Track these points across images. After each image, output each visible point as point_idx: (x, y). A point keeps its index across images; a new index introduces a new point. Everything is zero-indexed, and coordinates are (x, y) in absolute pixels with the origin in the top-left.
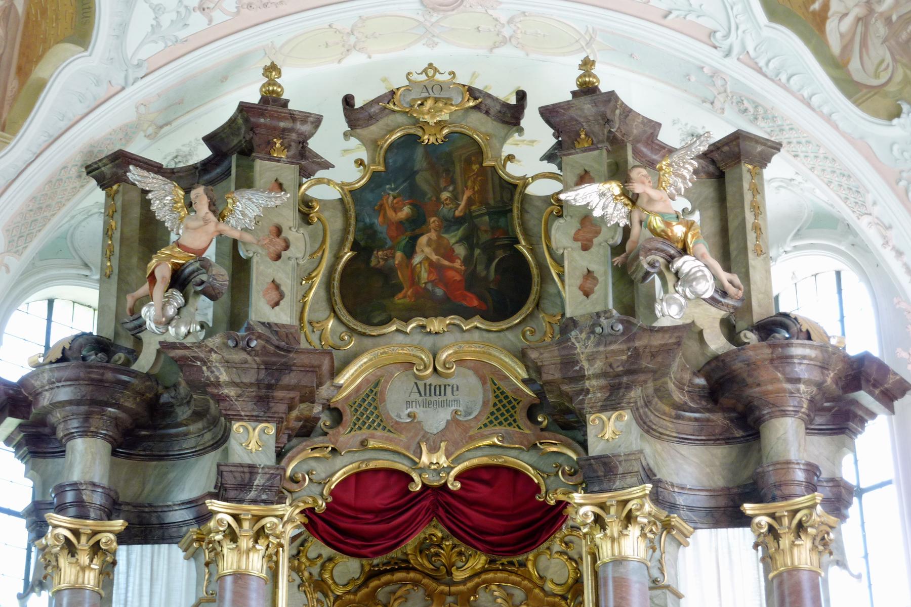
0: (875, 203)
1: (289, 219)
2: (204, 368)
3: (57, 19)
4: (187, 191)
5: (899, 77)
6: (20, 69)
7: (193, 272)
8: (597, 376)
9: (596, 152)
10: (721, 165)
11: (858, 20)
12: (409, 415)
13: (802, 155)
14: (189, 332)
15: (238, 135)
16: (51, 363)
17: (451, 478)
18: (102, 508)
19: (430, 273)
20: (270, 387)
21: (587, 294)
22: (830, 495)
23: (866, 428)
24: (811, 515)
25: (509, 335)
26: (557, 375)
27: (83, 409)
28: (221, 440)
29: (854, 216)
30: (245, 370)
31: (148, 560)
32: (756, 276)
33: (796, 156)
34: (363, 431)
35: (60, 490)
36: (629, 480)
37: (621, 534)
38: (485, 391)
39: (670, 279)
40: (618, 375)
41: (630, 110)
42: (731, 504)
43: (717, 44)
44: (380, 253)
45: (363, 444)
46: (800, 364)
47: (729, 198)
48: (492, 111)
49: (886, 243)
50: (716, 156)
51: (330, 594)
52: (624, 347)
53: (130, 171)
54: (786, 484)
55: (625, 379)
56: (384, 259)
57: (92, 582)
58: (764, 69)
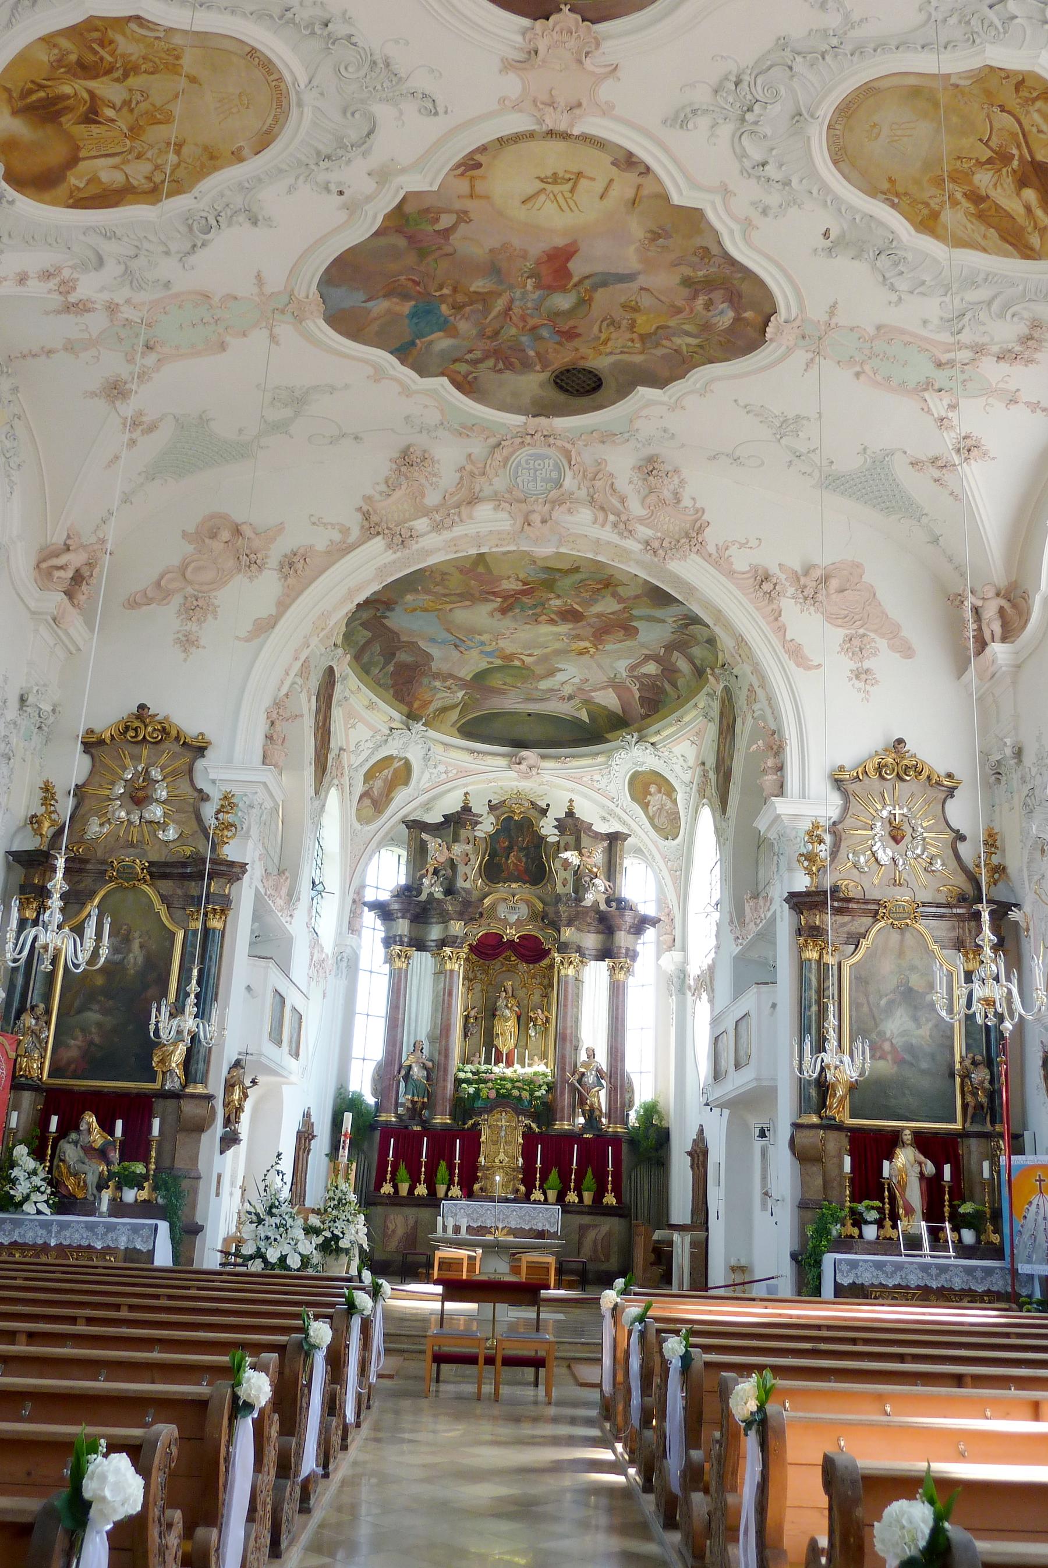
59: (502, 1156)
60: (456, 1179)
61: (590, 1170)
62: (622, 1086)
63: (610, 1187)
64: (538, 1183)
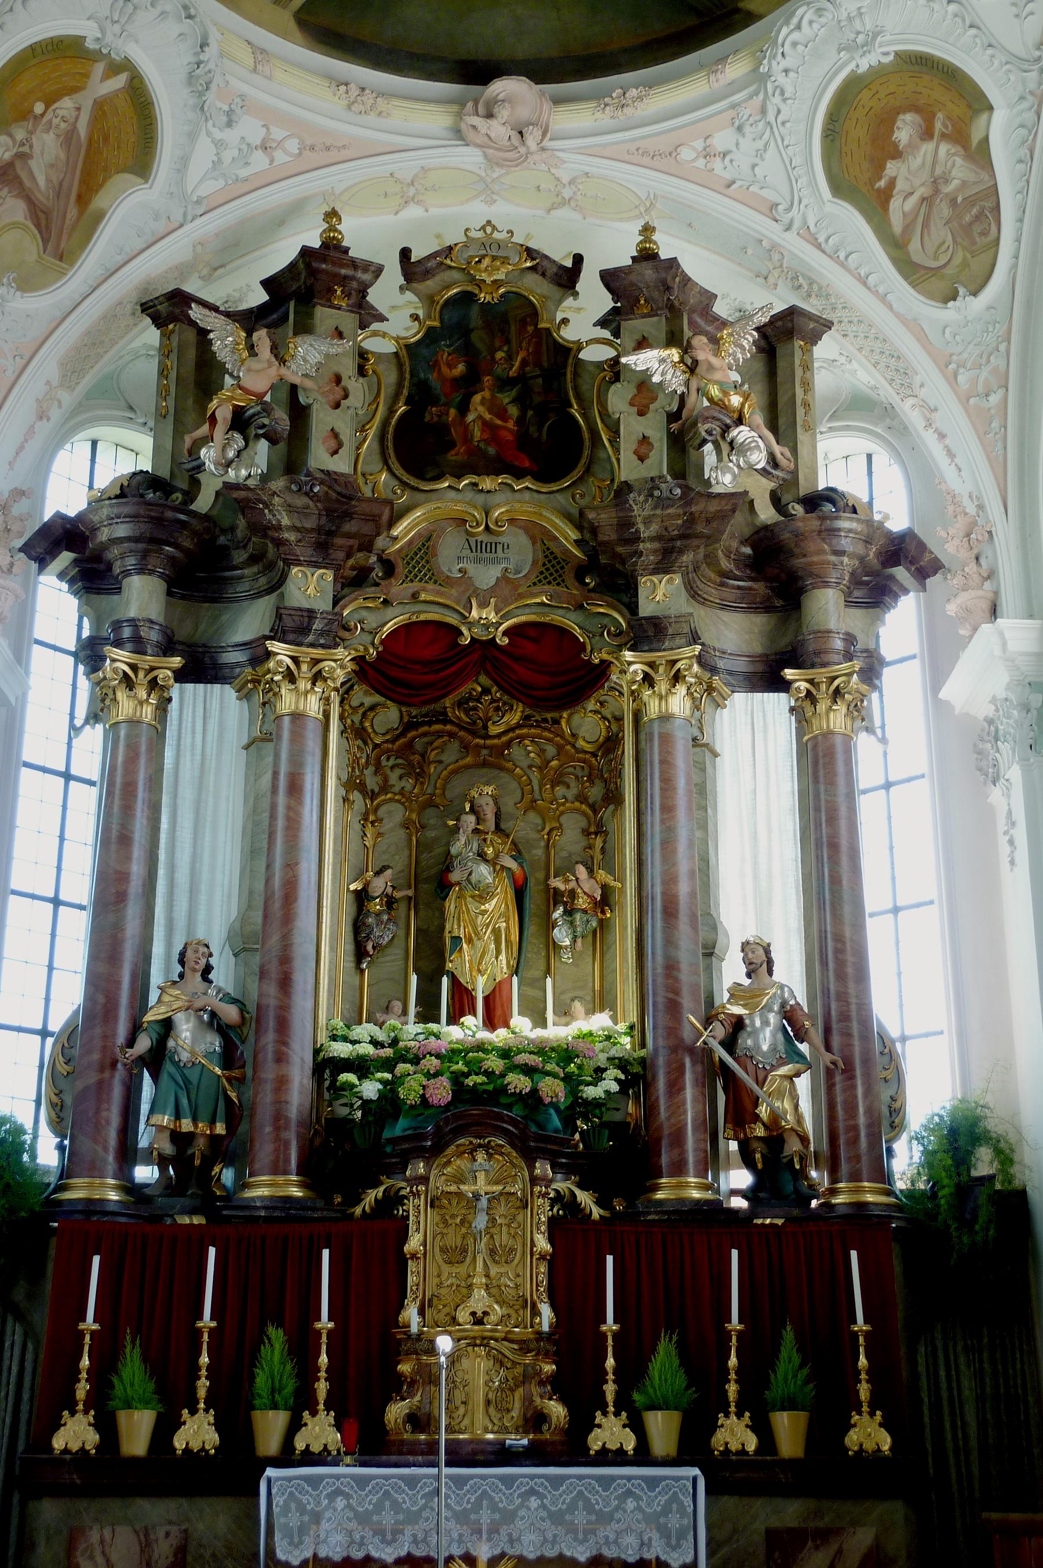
0: (922, 386)
1: (348, 368)
2: (266, 511)
3: (118, 147)
4: (249, 334)
5: (957, 260)
6: (79, 197)
7: (254, 415)
8: (652, 539)
9: (655, 319)
10: (773, 340)
11: (924, 200)
12: (460, 571)
13: (851, 335)
14: (250, 475)
15: (299, 280)
16: (110, 498)
17: (499, 634)
18: (158, 645)
19: (483, 431)
20: (330, 533)
21: (642, 459)
22: (864, 666)
23: (899, 603)
24: (849, 682)
25: (559, 497)
26: (614, 537)
27: (141, 546)
28: (277, 584)
29: (897, 398)
30: (307, 515)
31: (200, 699)
32: (803, 450)
33: (845, 336)
34: (414, 584)
35: (117, 626)
36: (678, 641)
37: (669, 692)
38: (535, 551)
39: (725, 448)
40: (672, 539)
41: (690, 279)
42: (768, 670)
43: (778, 218)
44: (434, 409)
45: (415, 596)
46: (846, 537)
47: (779, 372)
48: (548, 274)
49: (929, 424)
50: (769, 331)
51: (369, 742)
52: (680, 511)
53: (191, 308)
54: (826, 652)
55: (679, 543)
56: (438, 416)
57: (149, 716)
58: (823, 245)
59: (479, 1300)
60: (322, 1387)
61: (789, 1335)
62: (867, 1061)
63: (864, 1390)
64: (610, 1389)
